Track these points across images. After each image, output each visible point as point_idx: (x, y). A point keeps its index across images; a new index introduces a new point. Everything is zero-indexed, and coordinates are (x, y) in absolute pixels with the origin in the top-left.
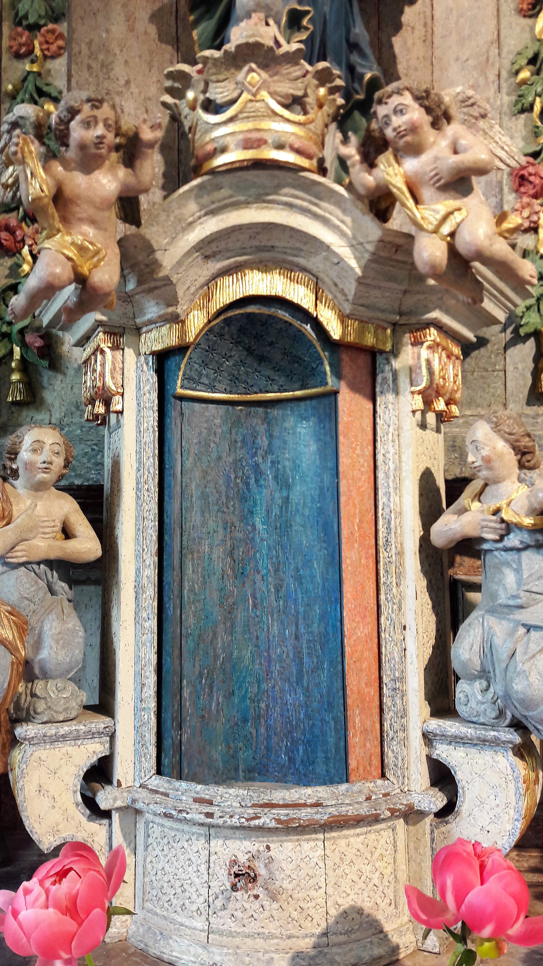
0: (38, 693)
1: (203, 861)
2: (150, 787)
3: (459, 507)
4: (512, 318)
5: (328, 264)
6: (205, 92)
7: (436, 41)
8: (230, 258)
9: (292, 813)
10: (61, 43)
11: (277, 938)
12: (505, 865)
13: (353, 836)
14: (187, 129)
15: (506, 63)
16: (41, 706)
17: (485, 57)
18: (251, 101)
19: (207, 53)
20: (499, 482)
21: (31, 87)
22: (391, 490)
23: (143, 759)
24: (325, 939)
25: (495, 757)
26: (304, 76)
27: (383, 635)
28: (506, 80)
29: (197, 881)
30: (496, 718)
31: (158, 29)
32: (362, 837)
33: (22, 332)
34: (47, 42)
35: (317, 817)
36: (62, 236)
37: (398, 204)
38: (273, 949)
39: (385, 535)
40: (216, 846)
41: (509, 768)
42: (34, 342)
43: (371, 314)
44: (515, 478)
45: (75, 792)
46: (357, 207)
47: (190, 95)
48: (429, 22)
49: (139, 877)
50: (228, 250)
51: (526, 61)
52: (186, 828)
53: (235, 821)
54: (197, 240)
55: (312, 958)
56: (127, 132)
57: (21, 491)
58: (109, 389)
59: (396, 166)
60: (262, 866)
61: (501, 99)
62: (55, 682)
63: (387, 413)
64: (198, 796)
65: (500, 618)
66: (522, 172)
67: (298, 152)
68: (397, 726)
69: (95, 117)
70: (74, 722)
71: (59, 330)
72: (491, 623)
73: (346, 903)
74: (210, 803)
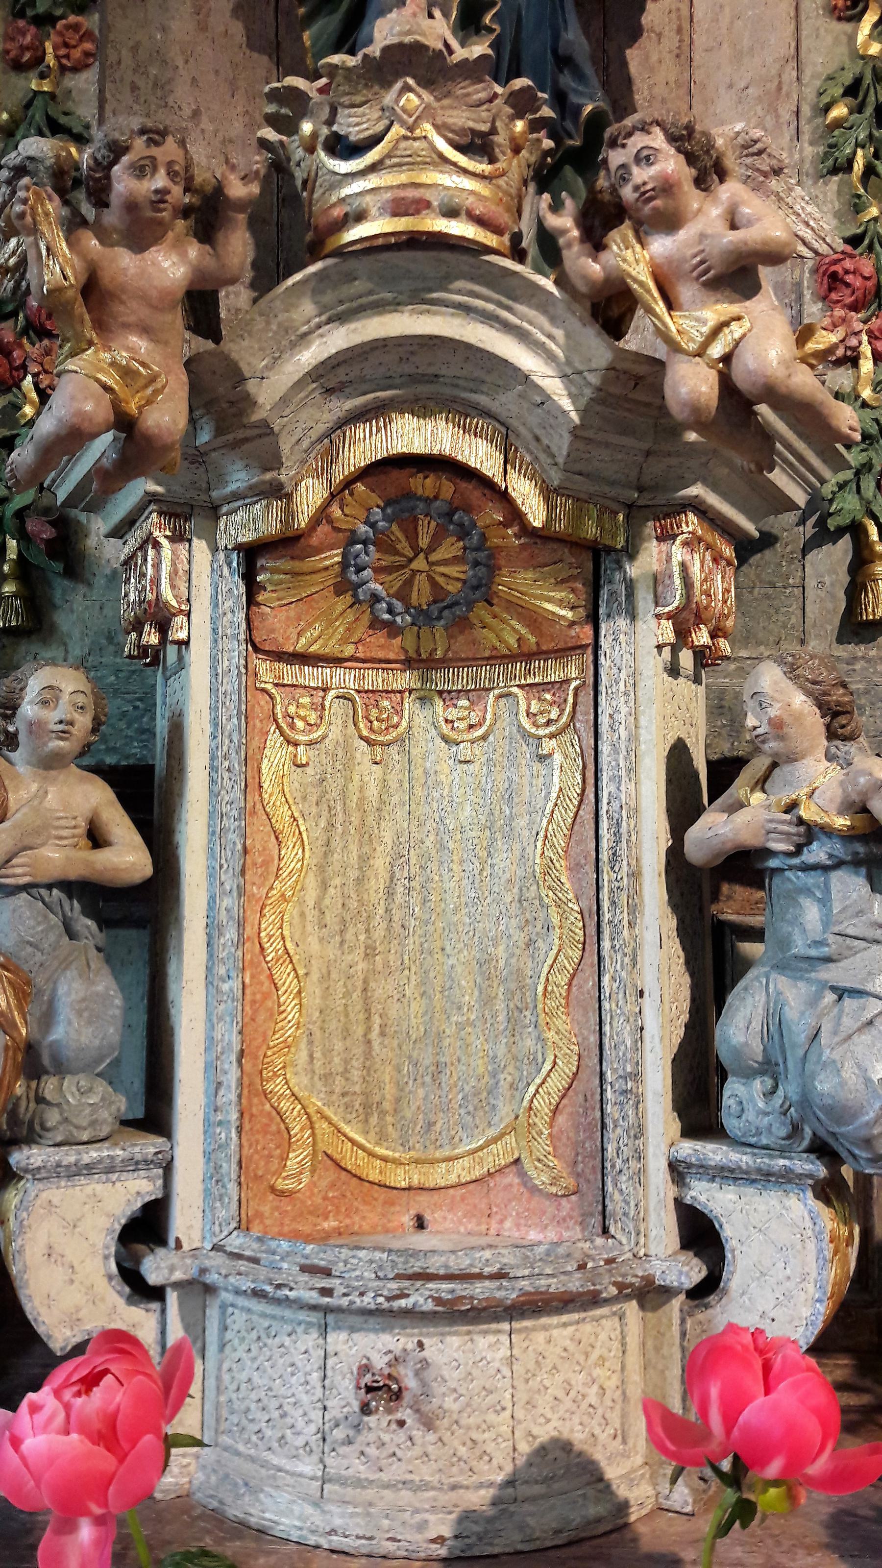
0: (48, 1097)
1: (316, 1366)
2: (228, 1249)
3: (731, 801)
4: (816, 501)
5: (525, 405)
6: (330, 122)
7: (696, 57)
8: (365, 393)
9: (460, 1288)
10: (88, 46)
11: (433, 1488)
12: (803, 1364)
13: (557, 1326)
14: (299, 183)
15: (810, 93)
16: (53, 1117)
17: (776, 83)
18: (405, 138)
19: (336, 59)
20: (796, 760)
21: (39, 117)
22: (623, 773)
23: (218, 1204)
24: (510, 1490)
25: (785, 1200)
26: (491, 101)
27: (606, 1005)
28: (809, 121)
29: (305, 1399)
30: (788, 1137)
31: (247, 29)
32: (571, 1329)
33: (20, 514)
34: (66, 45)
35: (499, 1294)
36: (96, 352)
37: (640, 312)
38: (427, 1507)
39: (611, 844)
40: (336, 1343)
41: (807, 1218)
42: (40, 532)
43: (593, 488)
44: (820, 753)
45: (106, 1257)
46: (574, 313)
47: (307, 127)
48: (686, 25)
49: (211, 1393)
50: (363, 380)
51: (841, 91)
52: (288, 1313)
53: (368, 1301)
54: (314, 362)
55: (490, 1520)
56: (202, 186)
57: (22, 769)
58: (166, 603)
59: (638, 247)
60: (411, 1374)
61: (801, 151)
62: (76, 1078)
63: (617, 648)
64: (308, 1262)
65: (795, 979)
66: (833, 268)
67: (480, 221)
68: (627, 1152)
69: (153, 159)
70: (106, 1144)
71: (83, 510)
72: (779, 986)
73: (544, 1433)
74: (327, 1273)
